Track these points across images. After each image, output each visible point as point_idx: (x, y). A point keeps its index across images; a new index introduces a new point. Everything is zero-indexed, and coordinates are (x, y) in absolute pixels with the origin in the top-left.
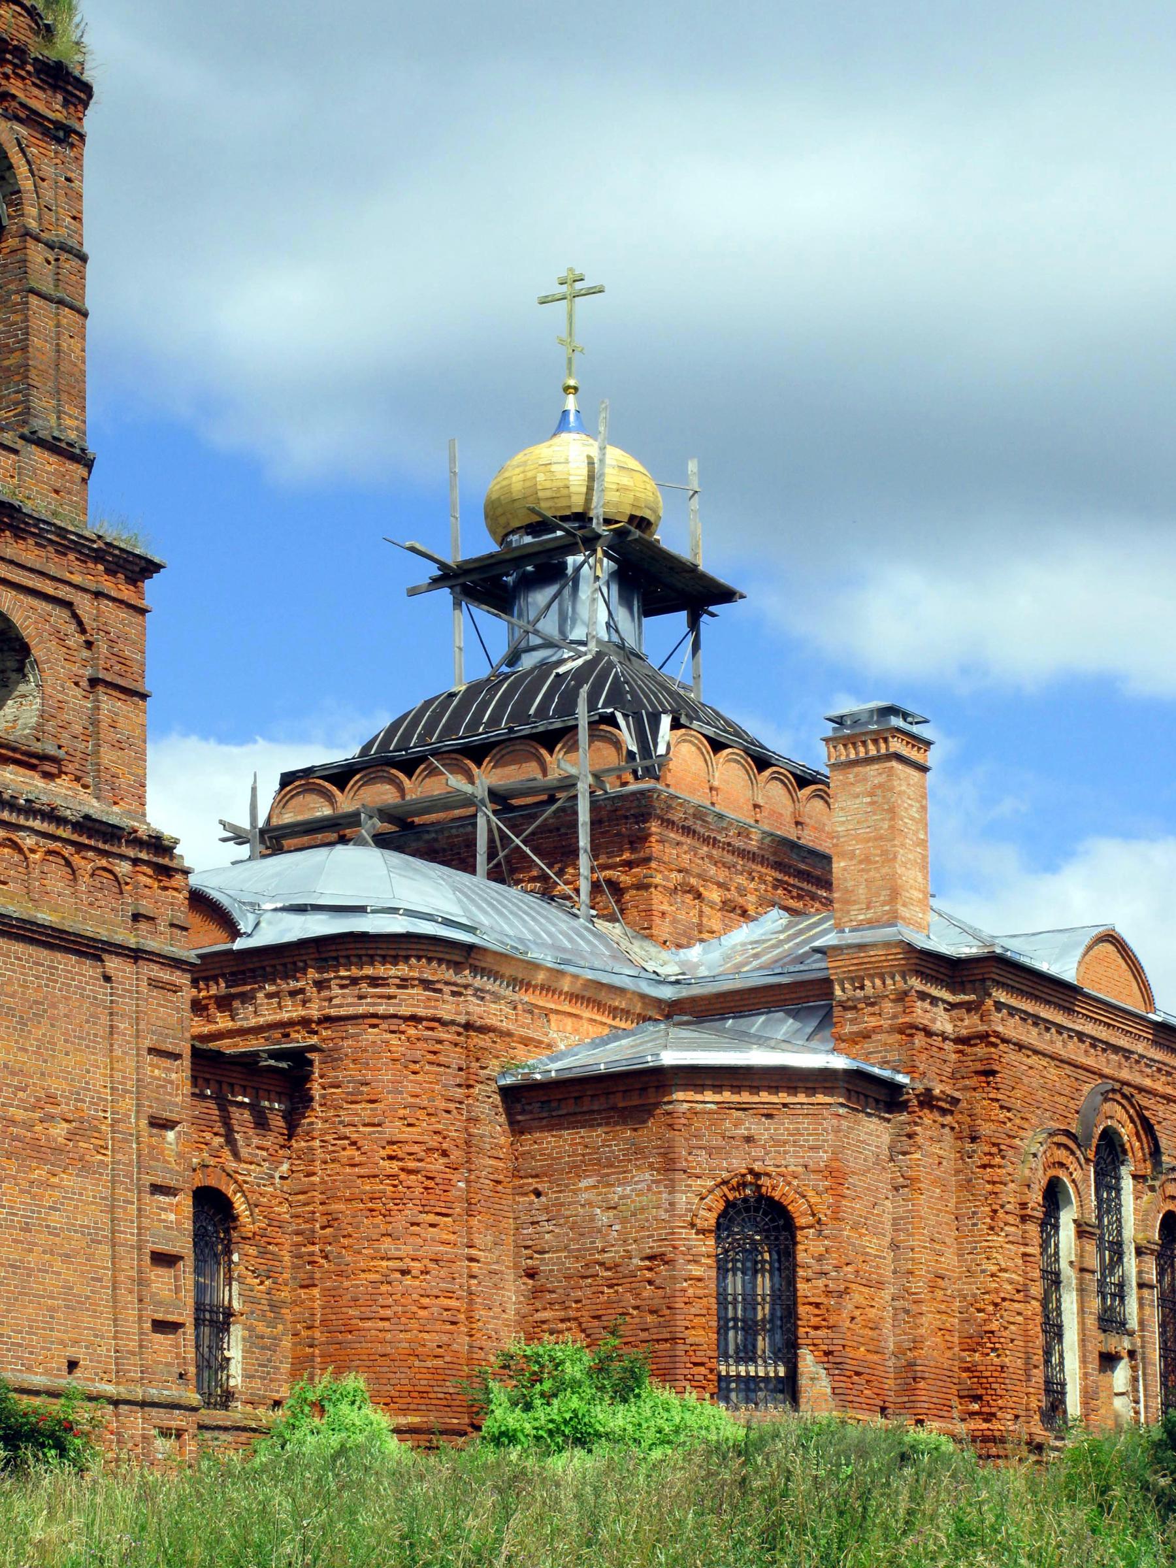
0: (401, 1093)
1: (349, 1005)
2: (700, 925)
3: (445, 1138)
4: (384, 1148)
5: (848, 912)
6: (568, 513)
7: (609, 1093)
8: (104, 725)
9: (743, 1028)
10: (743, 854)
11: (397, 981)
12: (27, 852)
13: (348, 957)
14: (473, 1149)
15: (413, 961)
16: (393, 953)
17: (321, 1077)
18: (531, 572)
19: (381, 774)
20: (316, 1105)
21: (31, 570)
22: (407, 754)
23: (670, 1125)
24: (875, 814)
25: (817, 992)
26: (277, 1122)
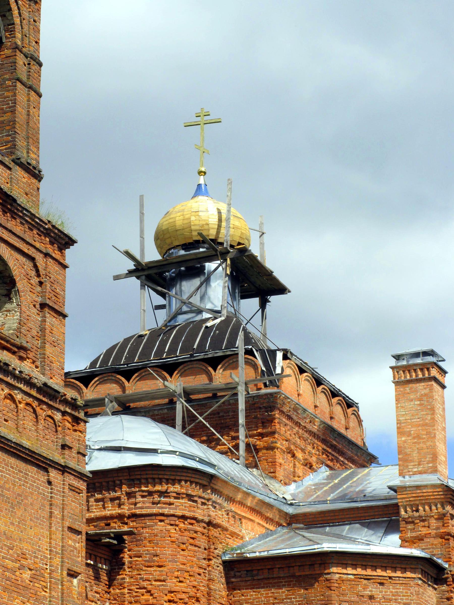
0: (176, 562)
1: (147, 508)
2: (294, 472)
3: (198, 590)
4: (166, 595)
5: (407, 466)
6: (191, 241)
7: (289, 567)
8: (47, 331)
9: (338, 532)
10: (311, 433)
11: (175, 495)
12: (18, 403)
13: (147, 479)
14: (212, 598)
15: (183, 483)
16: (173, 477)
17: (129, 550)
18: (183, 271)
19: (111, 378)
20: (126, 567)
21: (19, 237)
22: (128, 367)
23: (329, 587)
24: (423, 411)
25: (380, 513)
26: (104, 577)
